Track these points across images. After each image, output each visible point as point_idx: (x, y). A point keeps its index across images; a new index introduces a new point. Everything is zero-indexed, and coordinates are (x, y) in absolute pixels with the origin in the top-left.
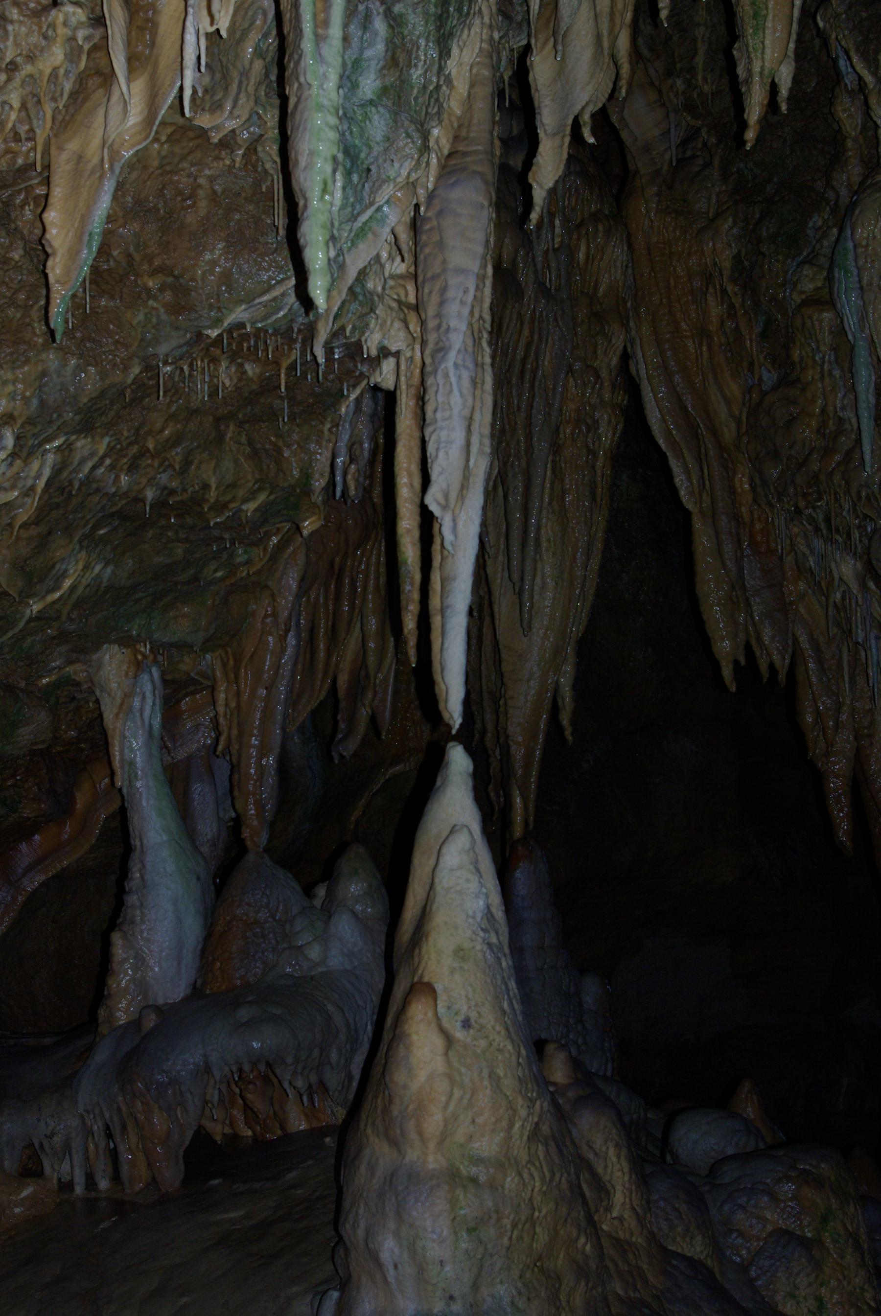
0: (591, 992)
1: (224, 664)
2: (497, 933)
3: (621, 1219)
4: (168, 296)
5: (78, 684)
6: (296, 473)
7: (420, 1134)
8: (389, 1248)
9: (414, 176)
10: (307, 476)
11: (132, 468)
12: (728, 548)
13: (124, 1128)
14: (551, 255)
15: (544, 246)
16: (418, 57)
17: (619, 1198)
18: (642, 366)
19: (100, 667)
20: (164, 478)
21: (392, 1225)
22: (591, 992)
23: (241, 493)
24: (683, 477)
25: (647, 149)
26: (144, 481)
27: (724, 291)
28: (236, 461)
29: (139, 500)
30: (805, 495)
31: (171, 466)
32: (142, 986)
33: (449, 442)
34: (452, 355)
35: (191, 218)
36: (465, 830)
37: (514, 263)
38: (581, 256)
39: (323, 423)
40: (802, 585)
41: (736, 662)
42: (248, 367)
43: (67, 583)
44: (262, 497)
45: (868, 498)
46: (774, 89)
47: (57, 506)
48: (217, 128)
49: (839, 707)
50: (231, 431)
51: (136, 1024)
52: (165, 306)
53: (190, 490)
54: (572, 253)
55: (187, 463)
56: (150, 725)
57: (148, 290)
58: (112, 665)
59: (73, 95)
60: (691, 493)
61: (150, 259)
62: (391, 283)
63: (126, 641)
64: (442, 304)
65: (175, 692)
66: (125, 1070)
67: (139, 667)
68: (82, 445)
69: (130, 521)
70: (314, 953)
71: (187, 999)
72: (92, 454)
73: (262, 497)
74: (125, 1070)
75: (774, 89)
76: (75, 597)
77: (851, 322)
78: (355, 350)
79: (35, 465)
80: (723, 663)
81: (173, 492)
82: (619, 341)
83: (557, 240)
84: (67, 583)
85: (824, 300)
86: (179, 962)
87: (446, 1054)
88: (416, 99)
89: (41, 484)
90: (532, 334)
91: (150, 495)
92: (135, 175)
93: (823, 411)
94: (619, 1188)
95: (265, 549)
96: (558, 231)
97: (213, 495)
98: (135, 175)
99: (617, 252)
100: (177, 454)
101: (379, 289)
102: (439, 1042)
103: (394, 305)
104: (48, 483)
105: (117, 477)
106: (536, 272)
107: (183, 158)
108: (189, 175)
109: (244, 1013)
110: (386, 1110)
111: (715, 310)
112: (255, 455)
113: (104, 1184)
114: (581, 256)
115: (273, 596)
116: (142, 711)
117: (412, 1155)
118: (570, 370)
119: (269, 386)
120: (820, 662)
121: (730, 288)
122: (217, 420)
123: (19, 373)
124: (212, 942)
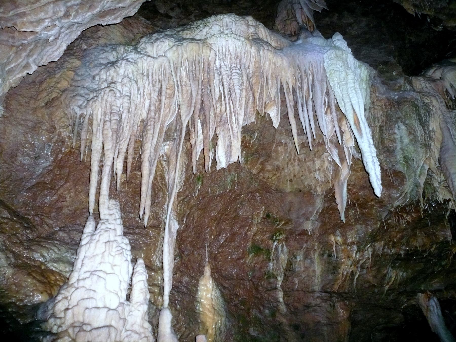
11: (394, 247)
16: (417, 130)
19: (419, 299)
20: (404, 247)
29: (401, 254)
31: (404, 244)
39: (444, 223)
44: (434, 246)
52: (378, 207)
56: (438, 314)
58: (421, 297)
63: (422, 292)
64: (452, 184)
67: (429, 299)
68: (377, 245)
69: (406, 260)
73: (434, 246)
81: (408, 250)
84: (393, 279)
88: (420, 139)
89: (370, 256)
91: (402, 252)
92: (357, 181)
95: (449, 259)
100: (404, 241)
104: (372, 255)
105: (391, 250)
112: (428, 236)
116: (434, 311)
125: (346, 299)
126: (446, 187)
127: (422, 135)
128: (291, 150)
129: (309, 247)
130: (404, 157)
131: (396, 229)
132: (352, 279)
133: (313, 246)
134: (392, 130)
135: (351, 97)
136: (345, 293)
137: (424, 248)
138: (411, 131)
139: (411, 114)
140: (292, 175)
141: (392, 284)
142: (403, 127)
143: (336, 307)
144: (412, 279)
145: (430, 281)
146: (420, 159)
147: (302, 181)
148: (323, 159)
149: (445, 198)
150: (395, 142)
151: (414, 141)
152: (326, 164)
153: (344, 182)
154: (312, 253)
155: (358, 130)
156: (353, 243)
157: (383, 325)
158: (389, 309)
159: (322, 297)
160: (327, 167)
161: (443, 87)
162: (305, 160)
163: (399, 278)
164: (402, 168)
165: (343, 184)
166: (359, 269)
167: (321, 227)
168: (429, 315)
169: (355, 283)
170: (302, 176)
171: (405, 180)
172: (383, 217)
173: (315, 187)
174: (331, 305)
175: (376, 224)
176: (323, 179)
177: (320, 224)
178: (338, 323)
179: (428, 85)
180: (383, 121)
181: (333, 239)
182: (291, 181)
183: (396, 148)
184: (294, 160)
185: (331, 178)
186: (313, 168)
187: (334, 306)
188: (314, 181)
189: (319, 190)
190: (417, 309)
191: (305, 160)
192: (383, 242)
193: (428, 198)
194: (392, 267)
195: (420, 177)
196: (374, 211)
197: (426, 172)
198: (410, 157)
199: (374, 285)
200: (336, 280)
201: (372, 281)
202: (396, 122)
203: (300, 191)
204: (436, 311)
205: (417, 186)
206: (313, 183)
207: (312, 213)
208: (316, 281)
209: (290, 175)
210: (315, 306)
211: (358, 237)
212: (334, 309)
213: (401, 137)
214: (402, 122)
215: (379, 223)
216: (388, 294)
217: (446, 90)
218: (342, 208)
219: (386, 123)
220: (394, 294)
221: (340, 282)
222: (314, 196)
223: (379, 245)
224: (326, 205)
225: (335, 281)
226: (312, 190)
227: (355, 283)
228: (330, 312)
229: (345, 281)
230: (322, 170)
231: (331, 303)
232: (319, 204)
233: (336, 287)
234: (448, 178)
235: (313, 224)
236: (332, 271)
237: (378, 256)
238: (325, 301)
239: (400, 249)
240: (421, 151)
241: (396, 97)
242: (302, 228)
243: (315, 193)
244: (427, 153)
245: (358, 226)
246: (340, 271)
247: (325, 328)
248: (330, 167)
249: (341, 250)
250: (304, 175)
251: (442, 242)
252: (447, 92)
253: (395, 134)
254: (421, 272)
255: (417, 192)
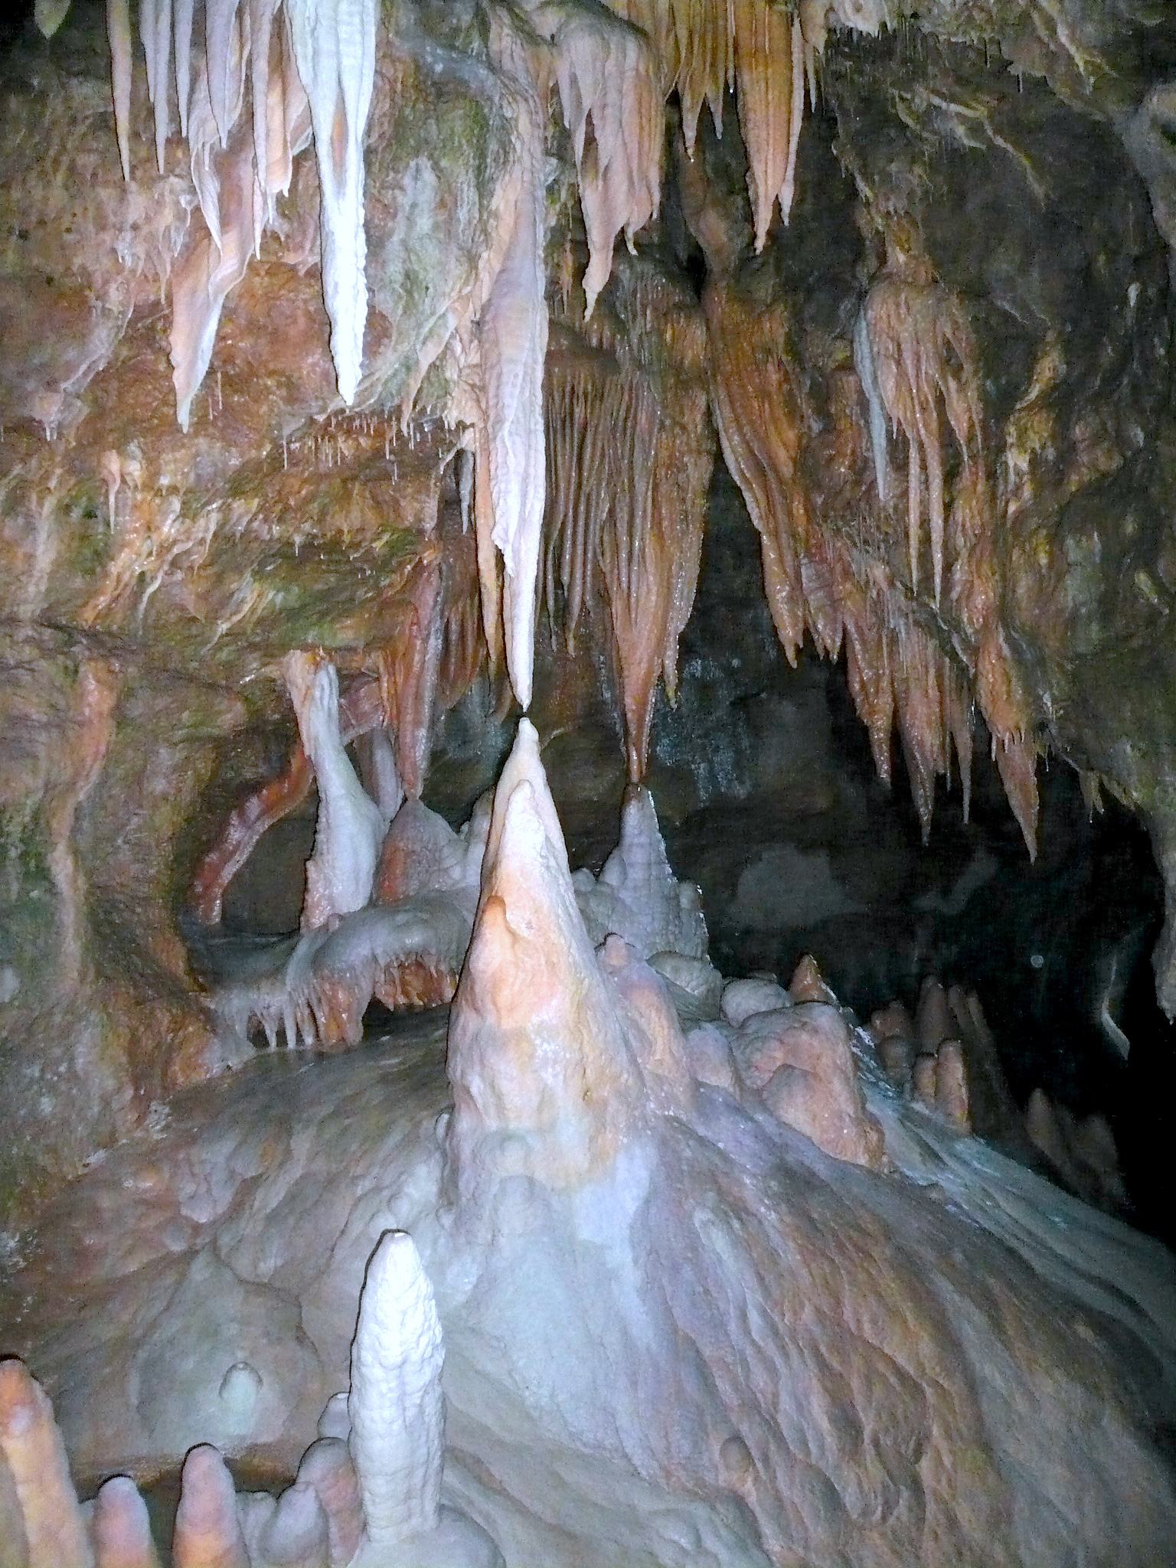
0: (688, 894)
1: (385, 661)
2: (555, 858)
3: (661, 1062)
4: (284, 392)
5: (274, 680)
6: (411, 519)
7: (495, 1004)
8: (476, 1085)
9: (466, 291)
10: (419, 520)
11: (281, 520)
12: (789, 558)
13: (320, 1000)
14: (645, 338)
15: (638, 331)
17: (659, 1046)
18: (720, 421)
20: (307, 527)
21: (477, 1068)
22: (688, 894)
23: (369, 535)
24: (754, 505)
25: (718, 252)
26: (291, 529)
27: (780, 362)
28: (362, 511)
29: (291, 545)
30: (843, 517)
32: (331, 900)
33: (507, 492)
34: (507, 425)
35: (293, 332)
36: (527, 785)
37: (612, 345)
38: (668, 336)
40: (848, 586)
41: (797, 646)
42: (362, 440)
43: (246, 608)
44: (386, 537)
45: (886, 518)
46: (777, 206)
47: (226, 552)
48: (303, 263)
49: (878, 678)
50: (357, 488)
51: (325, 927)
52: (282, 398)
53: (329, 535)
54: (661, 334)
55: (323, 513)
57: (267, 388)
58: (297, 664)
59: (186, 246)
60: (761, 517)
61: (265, 364)
62: (467, 371)
63: (305, 648)
64: (498, 387)
65: (349, 683)
66: (317, 961)
68: (238, 505)
69: (291, 561)
70: (456, 873)
71: (364, 909)
72: (247, 512)
73: (386, 537)
74: (317, 961)
75: (777, 206)
76: (255, 617)
77: (867, 384)
78: (439, 424)
79: (202, 522)
80: (787, 648)
81: (315, 537)
82: (702, 401)
83: (649, 326)
84: (246, 608)
85: (848, 366)
86: (357, 884)
87: (513, 947)
89: (209, 536)
90: (631, 398)
91: (298, 539)
93: (853, 452)
94: (660, 1041)
95: (402, 575)
96: (649, 318)
97: (347, 538)
98: (244, 302)
99: (698, 333)
100: (314, 508)
101: (455, 377)
102: (507, 939)
103: (467, 388)
104: (215, 535)
105: (270, 528)
106: (631, 349)
107: (282, 287)
108: (288, 300)
109: (401, 918)
110: (472, 988)
111: (774, 377)
112: (378, 504)
113: (309, 1040)
114: (668, 336)
115: (416, 609)
116: (321, 698)
117: (491, 1019)
118: (662, 426)
119: (378, 453)
120: (864, 642)
121: (784, 358)
122: (344, 481)
123: (178, 455)
124: (383, 867)
125: (112, 653)
126: (473, 386)
127: (470, 222)
128: (54, 123)
129: (29, 477)
130: (407, 276)
131: (303, 472)
132: (137, 595)
133: (46, 477)
134: (397, 172)
135: (343, 36)
136: (111, 634)
137: (359, 537)
138: (446, 202)
139: (464, 141)
140: (34, 219)
141: (240, 621)
142: (429, 176)
143: (80, 675)
144: (292, 614)
145: (333, 620)
146: (444, 294)
147: (63, 248)
148: (162, 195)
149: (462, 418)
150: (395, 216)
151: (446, 227)
152: (167, 217)
153: (215, 299)
154: (34, 497)
155: (335, 165)
156: (173, 490)
157: (185, 731)
158: (212, 686)
159: (43, 641)
160: (168, 228)
161: (551, 72)
162: (94, 175)
163: (262, 606)
164: (391, 305)
165: (208, 307)
166: (166, 567)
167: (89, 421)
168: (305, 710)
169: (142, 606)
170: (68, 230)
171: (386, 341)
172: (286, 432)
173: (106, 282)
174: (66, 668)
175: (260, 447)
176: (141, 263)
177: (86, 411)
178: (81, 725)
179: (517, 49)
180: (381, 136)
181: (113, 463)
182: (24, 235)
183: (390, 235)
184: (56, 162)
185: (169, 268)
186: (115, 214)
187: (76, 672)
188: (106, 262)
189: (115, 296)
190: (277, 693)
191: (94, 175)
192: (256, 501)
193: (424, 409)
194: (255, 573)
195: (424, 343)
196: (264, 408)
197: (448, 335)
198: (421, 277)
199: (194, 619)
200: (92, 593)
201: (191, 608)
202: (417, 152)
203: (50, 281)
204: (325, 702)
205: (408, 369)
206: (99, 267)
207: (70, 368)
208: (32, 589)
209: (25, 213)
210: (16, 667)
211: (192, 476)
212: (74, 681)
213: (414, 206)
214: (431, 157)
215: (268, 447)
216: (219, 647)
217: (556, 84)
218: (188, 385)
219: (389, 145)
220: (233, 648)
221: (103, 601)
222: (90, 312)
223: (244, 509)
224: (125, 352)
225: (90, 597)
226: (90, 288)
227: (142, 606)
228: (60, 690)
229: (116, 599)
230: (145, 230)
231: (69, 663)
232: (102, 344)
233: (89, 615)
234: (492, 367)
235: (67, 405)
236: (89, 565)
237: (229, 538)
238: (47, 653)
239: (297, 530)
240: (457, 269)
241: (439, 68)
242: (26, 413)
243: (99, 304)
244: (466, 283)
245: (202, 443)
246: (114, 568)
247: (43, 737)
248: (177, 229)
249: (130, 502)
250: (79, 232)
251: (407, 530)
252: (555, 91)
253: (402, 189)
254: (325, 595)
255: (404, 385)
